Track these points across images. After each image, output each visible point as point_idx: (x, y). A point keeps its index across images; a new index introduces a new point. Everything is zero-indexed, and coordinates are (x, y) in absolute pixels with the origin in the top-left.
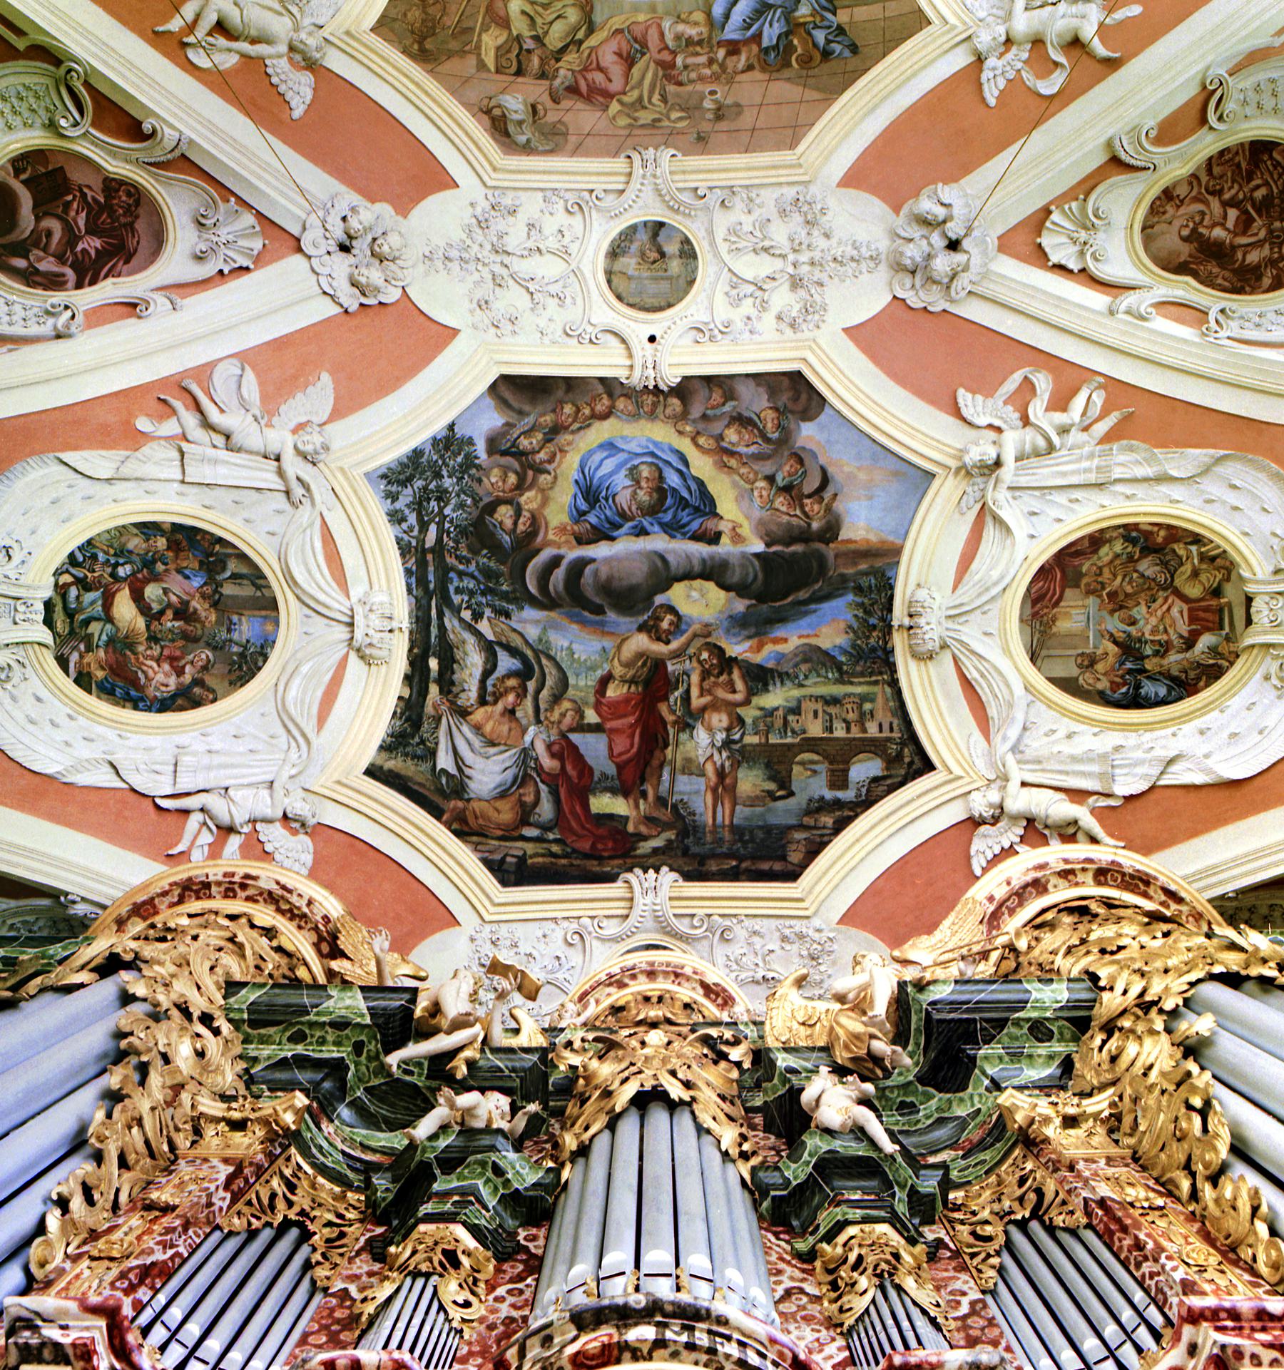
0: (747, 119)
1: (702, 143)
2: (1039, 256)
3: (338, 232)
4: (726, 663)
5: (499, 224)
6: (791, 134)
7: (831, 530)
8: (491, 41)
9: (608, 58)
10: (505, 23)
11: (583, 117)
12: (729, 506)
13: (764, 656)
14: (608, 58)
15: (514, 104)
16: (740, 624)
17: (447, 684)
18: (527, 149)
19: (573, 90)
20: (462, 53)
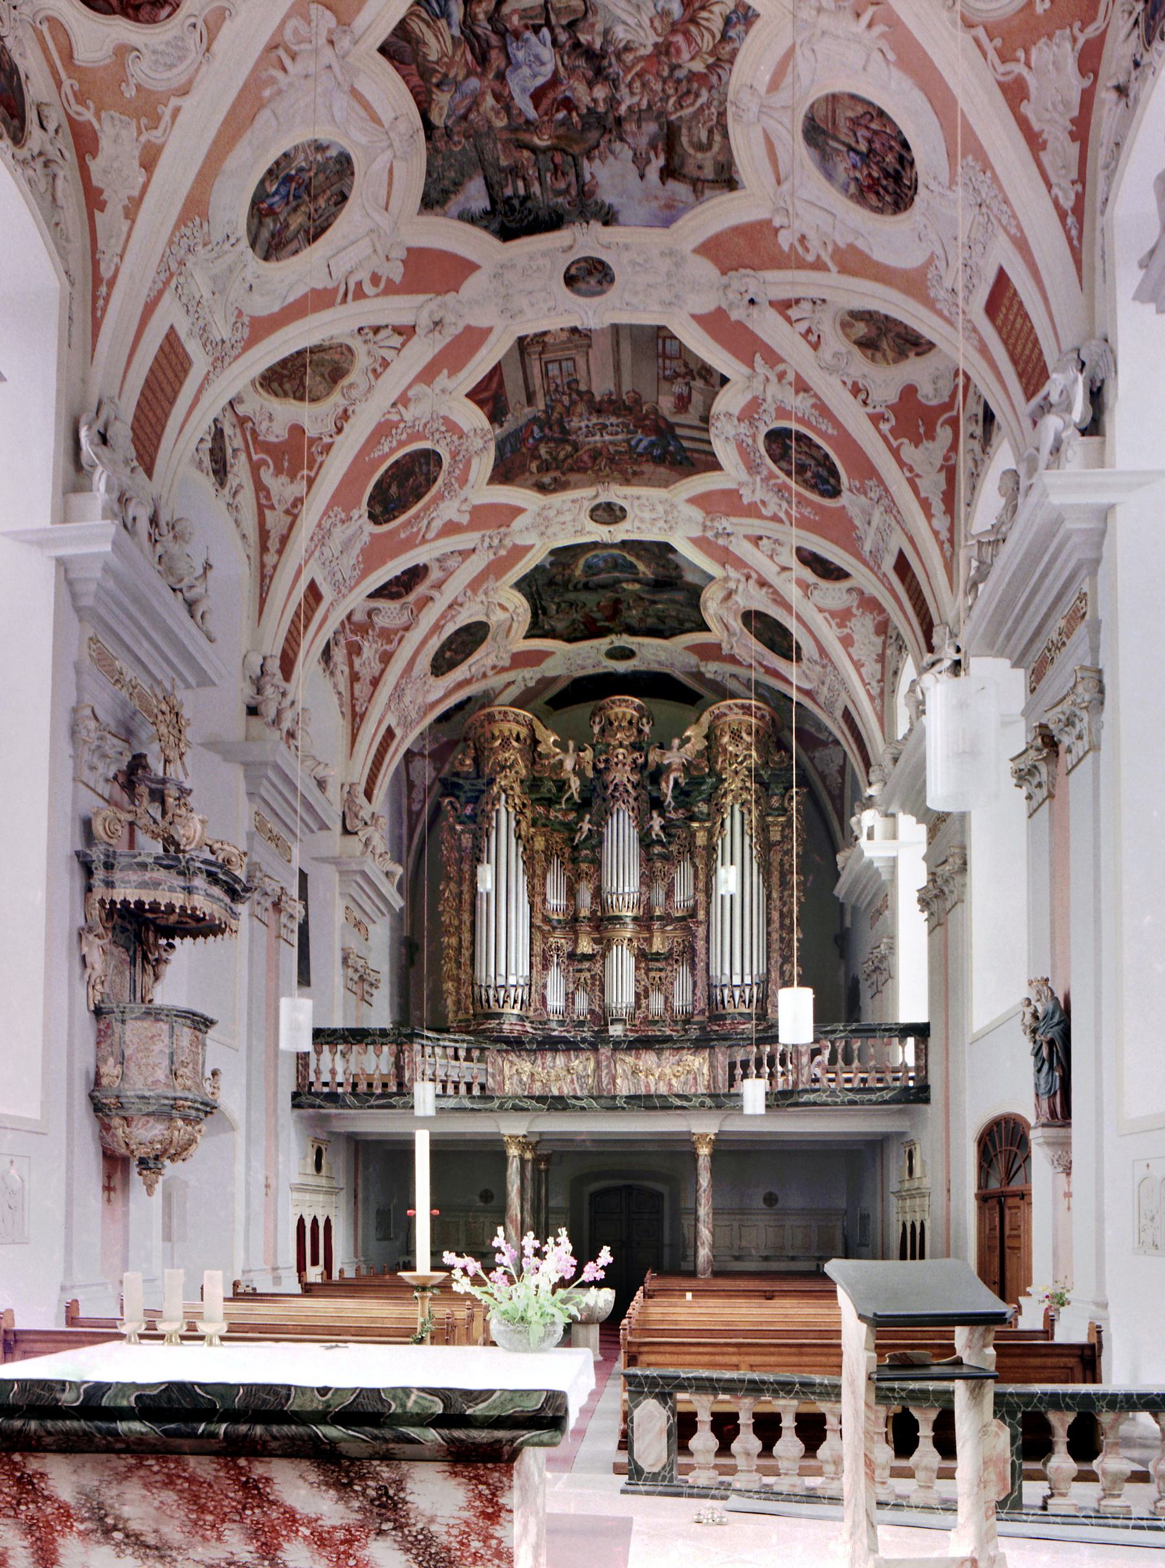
0: (646, 477)
1: (627, 482)
2: (757, 545)
3: (486, 544)
4: (641, 599)
5: (546, 513)
6: (665, 484)
7: (681, 577)
8: (534, 466)
9: (585, 458)
10: (540, 457)
11: (573, 477)
12: (641, 567)
13: (657, 597)
14: (585, 458)
15: (547, 479)
16: (648, 592)
17: (545, 613)
18: (555, 491)
19: (572, 470)
20: (523, 473)
